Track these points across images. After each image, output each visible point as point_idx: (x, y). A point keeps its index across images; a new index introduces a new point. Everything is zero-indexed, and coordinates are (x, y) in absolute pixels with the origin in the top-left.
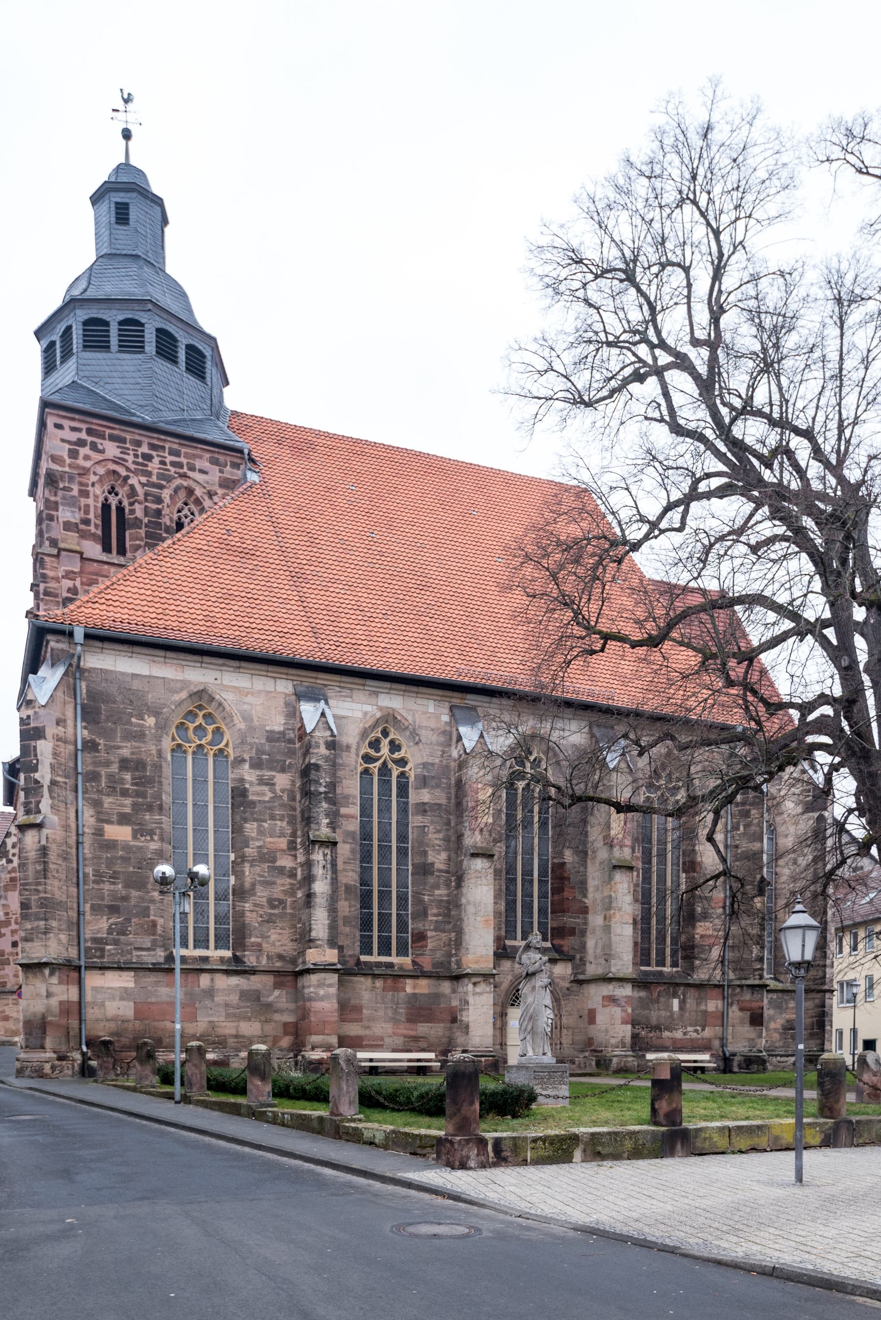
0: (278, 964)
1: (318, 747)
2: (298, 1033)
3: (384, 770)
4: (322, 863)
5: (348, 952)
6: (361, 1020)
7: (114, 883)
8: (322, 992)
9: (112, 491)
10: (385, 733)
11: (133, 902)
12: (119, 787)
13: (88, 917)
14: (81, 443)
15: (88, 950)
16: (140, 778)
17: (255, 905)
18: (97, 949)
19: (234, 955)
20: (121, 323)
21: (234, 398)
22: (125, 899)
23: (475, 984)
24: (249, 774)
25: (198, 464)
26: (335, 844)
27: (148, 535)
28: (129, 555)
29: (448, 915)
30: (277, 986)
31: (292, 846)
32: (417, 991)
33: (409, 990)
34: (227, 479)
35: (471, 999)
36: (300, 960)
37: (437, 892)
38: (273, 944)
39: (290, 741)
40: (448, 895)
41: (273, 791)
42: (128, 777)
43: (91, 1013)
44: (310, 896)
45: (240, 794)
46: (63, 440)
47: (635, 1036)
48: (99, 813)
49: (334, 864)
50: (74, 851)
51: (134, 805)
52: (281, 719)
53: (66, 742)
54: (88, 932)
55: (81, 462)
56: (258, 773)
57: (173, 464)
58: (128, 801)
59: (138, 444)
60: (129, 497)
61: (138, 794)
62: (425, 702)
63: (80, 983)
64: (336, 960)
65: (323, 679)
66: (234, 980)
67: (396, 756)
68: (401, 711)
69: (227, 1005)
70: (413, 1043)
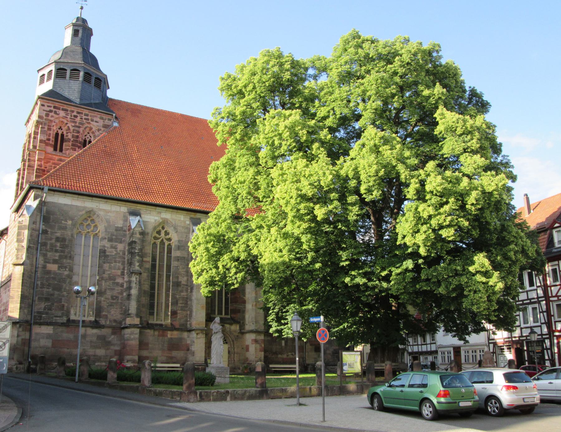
0: (114, 324)
1: (136, 234)
2: (121, 354)
3: (162, 243)
4: (135, 281)
5: (144, 319)
6: (147, 349)
7: (48, 288)
8: (132, 337)
9: (60, 128)
10: (163, 228)
11: (56, 296)
12: (54, 248)
13: (36, 302)
14: (51, 111)
15: (35, 316)
16: (63, 245)
17: (106, 298)
18: (38, 316)
19: (96, 320)
20: (71, 70)
21: (111, 94)
22: (53, 295)
23: (197, 334)
24: (107, 244)
25: (95, 119)
26: (141, 274)
27: (73, 145)
28: (64, 152)
29: (186, 304)
30: (114, 333)
31: (123, 273)
32: (173, 337)
33: (169, 336)
34: (105, 125)
35: (195, 341)
36: (123, 323)
37: (182, 294)
38: (112, 315)
39: (125, 231)
40: (187, 295)
41: (116, 251)
42: (58, 244)
43: (34, 344)
44: (129, 295)
45: (103, 252)
46: (44, 110)
47: (265, 357)
48: (45, 259)
49: (140, 282)
50: (34, 275)
51: (60, 256)
52: (121, 222)
53: (36, 231)
54: (35, 309)
55: (50, 118)
56: (111, 243)
57: (85, 119)
58: (58, 254)
59: (73, 112)
60: (66, 130)
61: (62, 251)
62: (180, 216)
63: (30, 331)
64: (138, 323)
65: (139, 207)
66: (95, 331)
67: (167, 237)
68: (171, 220)
69: (91, 342)
70: (170, 360)
